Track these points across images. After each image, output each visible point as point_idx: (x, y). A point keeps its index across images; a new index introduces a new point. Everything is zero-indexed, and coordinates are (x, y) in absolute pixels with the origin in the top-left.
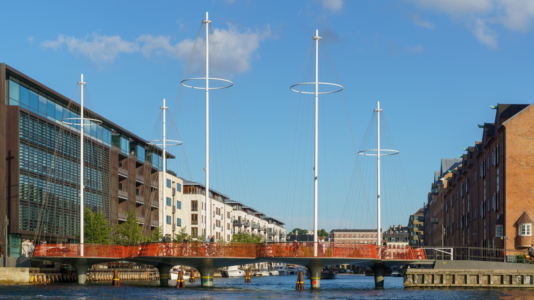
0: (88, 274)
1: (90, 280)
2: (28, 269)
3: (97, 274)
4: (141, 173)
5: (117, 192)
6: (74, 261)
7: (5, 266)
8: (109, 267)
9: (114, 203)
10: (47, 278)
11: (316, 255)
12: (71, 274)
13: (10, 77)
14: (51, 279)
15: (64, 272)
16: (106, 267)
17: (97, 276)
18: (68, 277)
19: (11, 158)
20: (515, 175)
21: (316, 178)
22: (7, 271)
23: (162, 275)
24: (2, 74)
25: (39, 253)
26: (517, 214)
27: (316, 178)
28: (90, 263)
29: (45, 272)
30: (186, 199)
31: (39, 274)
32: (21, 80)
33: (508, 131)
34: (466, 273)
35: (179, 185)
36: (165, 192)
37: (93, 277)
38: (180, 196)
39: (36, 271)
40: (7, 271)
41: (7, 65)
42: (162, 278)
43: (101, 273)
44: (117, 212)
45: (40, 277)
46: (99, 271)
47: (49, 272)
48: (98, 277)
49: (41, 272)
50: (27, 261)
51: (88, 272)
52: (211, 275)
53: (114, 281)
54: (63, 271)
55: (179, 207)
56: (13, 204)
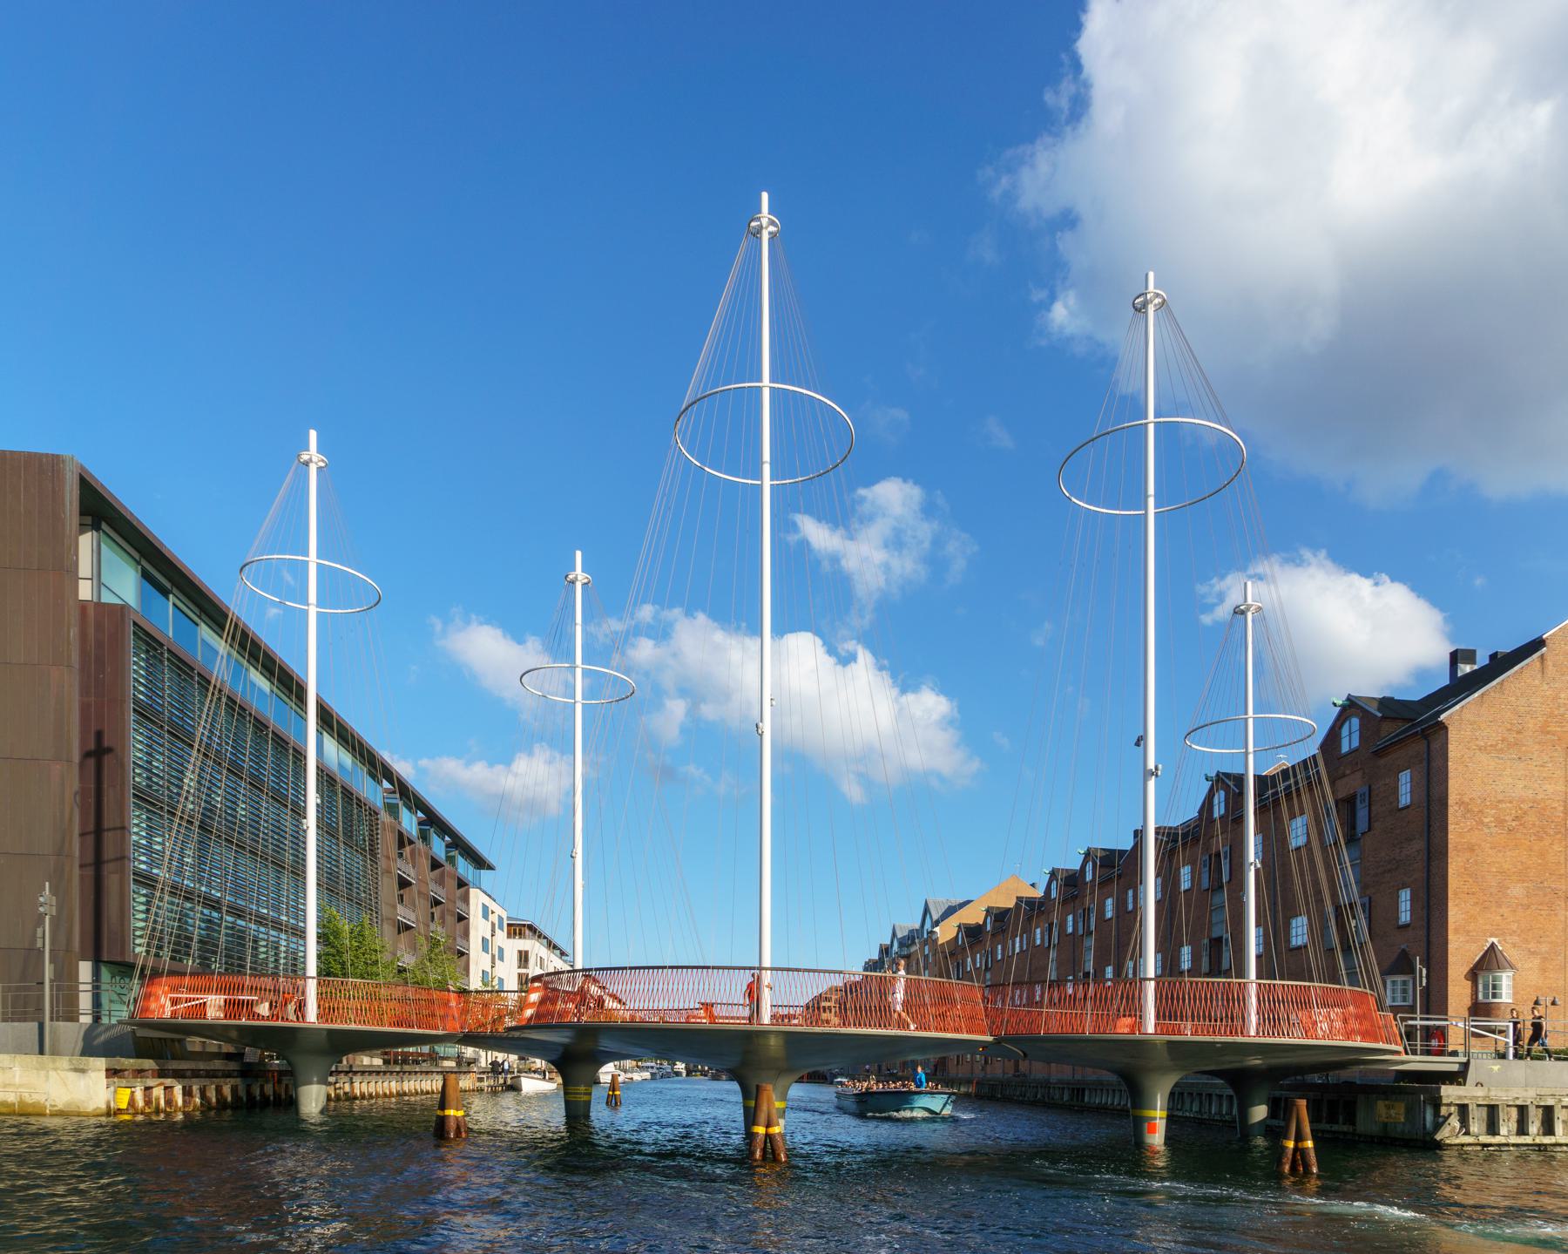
0: (332, 1079)
1: (338, 1098)
2: (101, 1063)
3: (357, 1079)
4: (440, 882)
5: (394, 907)
6: (283, 1039)
7: (41, 1052)
8: (386, 1062)
9: (388, 930)
10: (187, 1093)
11: (1151, 1029)
12: (280, 1082)
13: (104, 526)
14: (203, 1095)
15: (254, 1079)
16: (378, 1062)
17: (356, 1085)
18: (269, 1089)
19: (100, 754)
20: (1471, 849)
21: (1148, 774)
22: (17, 1069)
23: (572, 1089)
24: (68, 488)
25: (146, 1010)
26: (1474, 947)
27: (1148, 774)
28: (341, 1044)
29: (178, 1075)
30: (513, 946)
31: (151, 1082)
32: (142, 555)
33: (1453, 735)
34: (1550, 1102)
35: (500, 918)
36: (479, 928)
37: (347, 1088)
38: (501, 937)
39: (139, 1073)
40: (17, 1069)
41: (82, 468)
42: (571, 1098)
43: (367, 1078)
44: (396, 948)
45: (158, 1092)
46: (363, 1073)
47: (196, 1074)
48: (361, 1086)
49: (162, 1074)
50: (121, 1037)
51: (331, 1074)
52: (784, 1097)
53: (442, 1120)
54: (249, 1072)
55: (501, 959)
56: (111, 881)
